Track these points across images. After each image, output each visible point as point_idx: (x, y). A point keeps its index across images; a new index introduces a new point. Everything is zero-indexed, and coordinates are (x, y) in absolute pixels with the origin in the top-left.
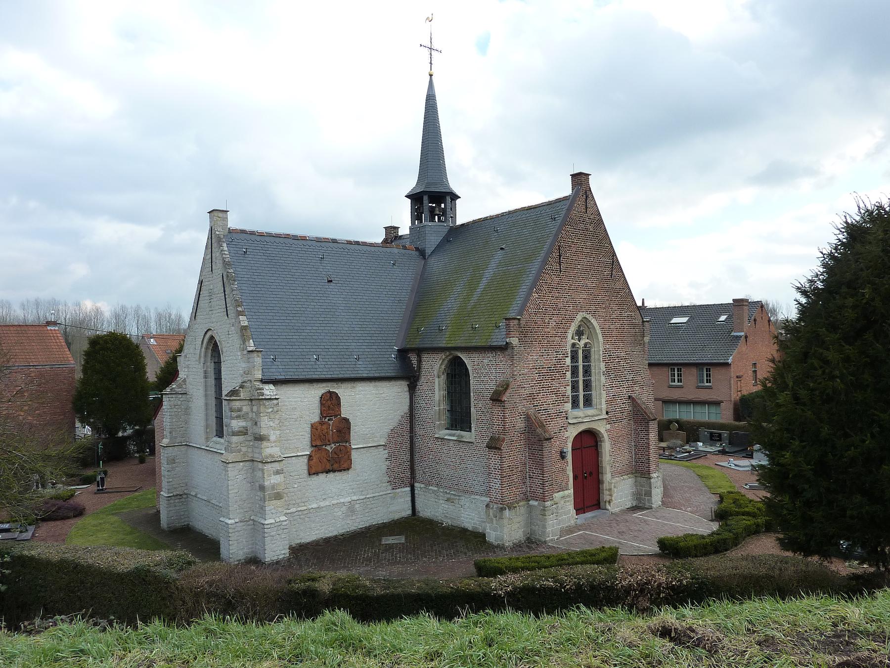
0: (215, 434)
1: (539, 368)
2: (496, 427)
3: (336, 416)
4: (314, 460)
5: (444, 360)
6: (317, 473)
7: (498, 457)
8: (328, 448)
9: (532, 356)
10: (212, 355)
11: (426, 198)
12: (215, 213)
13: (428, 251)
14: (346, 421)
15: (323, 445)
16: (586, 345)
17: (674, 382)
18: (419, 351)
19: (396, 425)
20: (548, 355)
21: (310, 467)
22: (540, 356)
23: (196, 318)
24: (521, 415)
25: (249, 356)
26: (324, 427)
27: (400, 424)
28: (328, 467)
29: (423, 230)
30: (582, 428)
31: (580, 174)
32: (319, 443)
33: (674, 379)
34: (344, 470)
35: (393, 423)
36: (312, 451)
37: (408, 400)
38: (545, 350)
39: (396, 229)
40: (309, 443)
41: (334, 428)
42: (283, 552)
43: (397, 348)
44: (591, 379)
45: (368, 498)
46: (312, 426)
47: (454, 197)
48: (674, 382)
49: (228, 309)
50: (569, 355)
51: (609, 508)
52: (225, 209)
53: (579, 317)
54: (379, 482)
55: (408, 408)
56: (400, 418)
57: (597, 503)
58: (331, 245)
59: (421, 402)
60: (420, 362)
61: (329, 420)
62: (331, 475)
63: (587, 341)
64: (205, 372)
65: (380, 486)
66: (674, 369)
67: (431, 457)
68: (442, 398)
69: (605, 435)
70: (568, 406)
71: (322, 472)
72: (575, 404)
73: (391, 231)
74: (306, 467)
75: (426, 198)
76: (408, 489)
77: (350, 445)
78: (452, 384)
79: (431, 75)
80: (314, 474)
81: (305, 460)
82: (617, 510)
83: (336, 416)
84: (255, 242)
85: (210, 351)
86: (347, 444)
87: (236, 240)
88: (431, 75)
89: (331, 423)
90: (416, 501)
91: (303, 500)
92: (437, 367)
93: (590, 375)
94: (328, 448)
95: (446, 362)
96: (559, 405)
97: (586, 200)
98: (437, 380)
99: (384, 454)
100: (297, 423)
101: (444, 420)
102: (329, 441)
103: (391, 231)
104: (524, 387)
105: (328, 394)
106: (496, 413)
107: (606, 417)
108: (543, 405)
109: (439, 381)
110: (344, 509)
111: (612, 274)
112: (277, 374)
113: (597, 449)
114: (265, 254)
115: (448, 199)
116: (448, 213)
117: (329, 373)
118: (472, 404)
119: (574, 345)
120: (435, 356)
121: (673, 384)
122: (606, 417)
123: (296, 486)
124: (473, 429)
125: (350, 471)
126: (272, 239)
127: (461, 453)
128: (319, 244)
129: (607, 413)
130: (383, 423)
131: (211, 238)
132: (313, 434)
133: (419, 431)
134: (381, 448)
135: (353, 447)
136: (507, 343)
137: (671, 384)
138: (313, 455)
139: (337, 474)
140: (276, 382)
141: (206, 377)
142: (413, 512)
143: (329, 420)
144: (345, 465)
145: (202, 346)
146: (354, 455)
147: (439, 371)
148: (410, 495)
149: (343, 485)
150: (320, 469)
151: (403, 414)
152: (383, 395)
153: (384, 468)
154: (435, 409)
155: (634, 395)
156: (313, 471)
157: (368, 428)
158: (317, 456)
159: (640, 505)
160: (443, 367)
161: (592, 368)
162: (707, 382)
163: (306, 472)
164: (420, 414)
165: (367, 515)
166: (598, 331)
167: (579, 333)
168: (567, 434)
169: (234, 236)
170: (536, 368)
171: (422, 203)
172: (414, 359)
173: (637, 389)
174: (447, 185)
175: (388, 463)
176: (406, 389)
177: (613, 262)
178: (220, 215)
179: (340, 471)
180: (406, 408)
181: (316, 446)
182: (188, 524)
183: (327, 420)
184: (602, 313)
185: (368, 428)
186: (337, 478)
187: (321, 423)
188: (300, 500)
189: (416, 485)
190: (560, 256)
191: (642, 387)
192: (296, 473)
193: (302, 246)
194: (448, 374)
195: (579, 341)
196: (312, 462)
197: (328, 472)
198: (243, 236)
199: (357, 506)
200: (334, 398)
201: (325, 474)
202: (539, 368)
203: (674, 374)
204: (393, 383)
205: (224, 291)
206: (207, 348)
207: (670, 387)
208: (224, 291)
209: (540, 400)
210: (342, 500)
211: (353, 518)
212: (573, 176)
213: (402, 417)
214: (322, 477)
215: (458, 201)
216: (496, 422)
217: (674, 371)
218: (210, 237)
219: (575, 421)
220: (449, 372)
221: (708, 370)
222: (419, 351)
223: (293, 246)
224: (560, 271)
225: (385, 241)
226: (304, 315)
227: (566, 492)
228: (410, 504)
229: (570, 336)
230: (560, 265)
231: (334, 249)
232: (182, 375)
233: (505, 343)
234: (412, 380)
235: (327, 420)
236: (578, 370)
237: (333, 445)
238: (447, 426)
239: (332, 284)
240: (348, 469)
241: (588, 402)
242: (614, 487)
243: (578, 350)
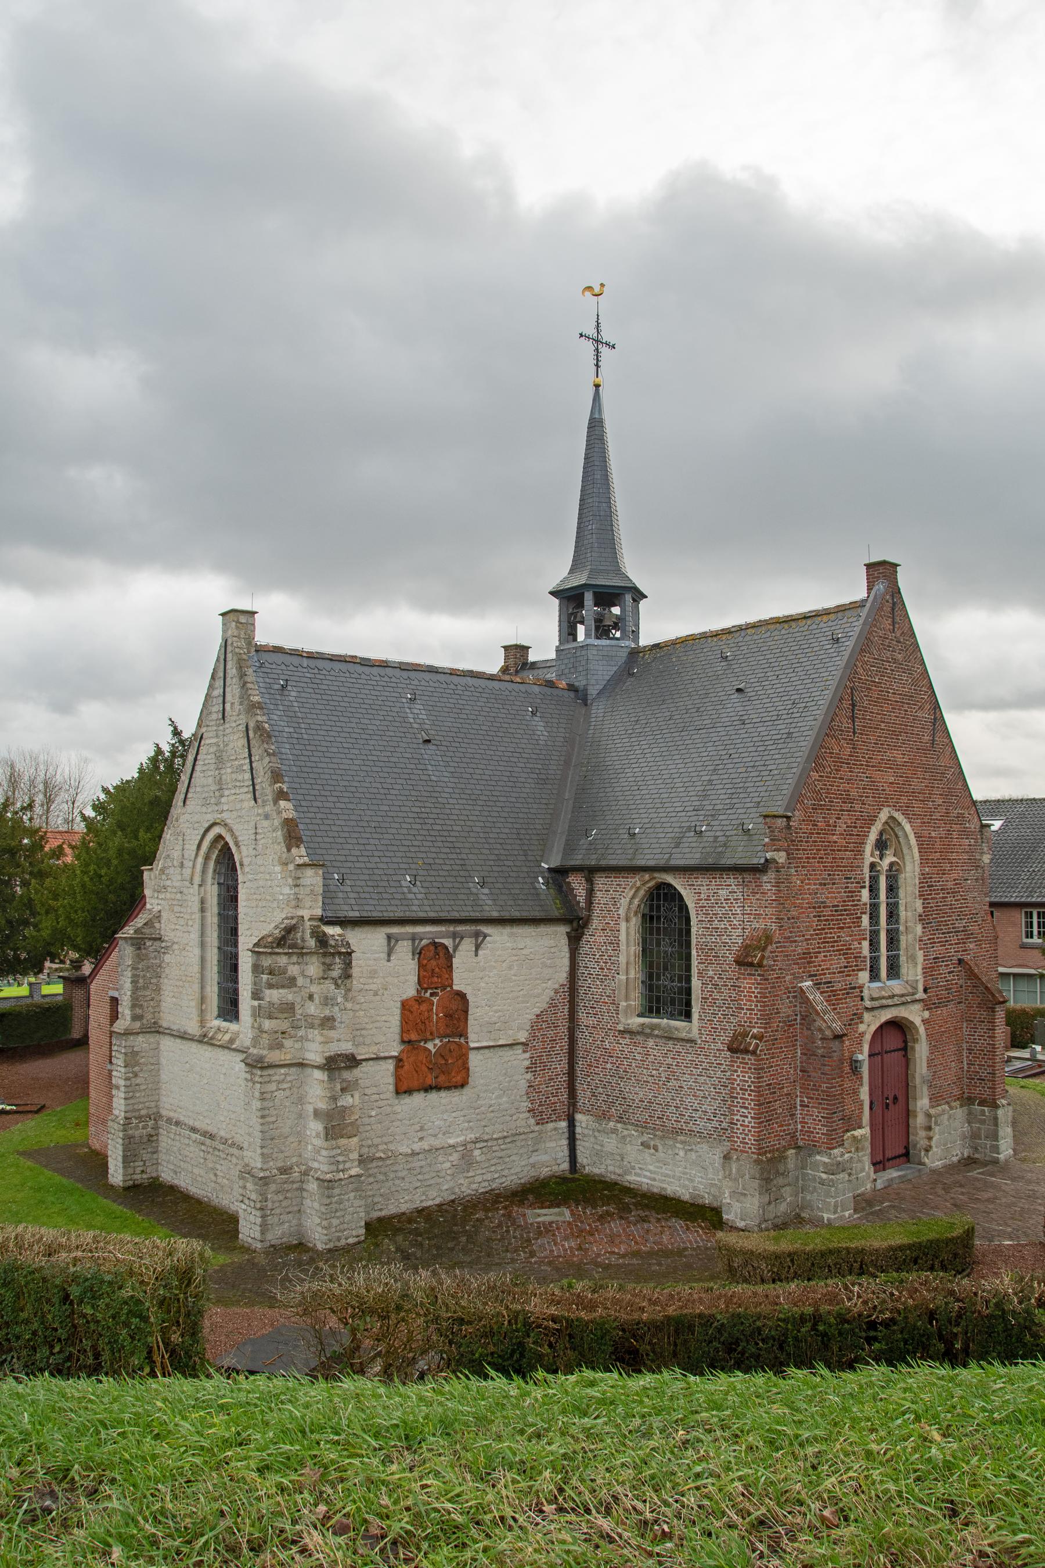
0: (216, 1013)
1: (819, 907)
2: (745, 1014)
3: (444, 988)
4: (405, 1068)
5: (638, 889)
6: (409, 1092)
7: (750, 1068)
8: (430, 1046)
9: (809, 884)
10: (215, 871)
11: (589, 598)
12: (231, 616)
13: (593, 691)
14: (462, 996)
15: (420, 1041)
16: (892, 864)
17: (1032, 937)
18: (590, 872)
19: (545, 1006)
20: (834, 884)
21: (398, 1079)
22: (821, 884)
23: (188, 802)
24: (790, 992)
25: (299, 874)
26: (424, 1007)
27: (552, 1005)
28: (430, 1080)
29: (583, 653)
30: (886, 1016)
31: (883, 563)
32: (414, 1036)
33: (1032, 932)
34: (456, 1087)
35: (541, 1004)
36: (402, 1051)
37: (566, 962)
38: (829, 875)
39: (524, 649)
40: (397, 1037)
41: (440, 1009)
42: (354, 1233)
43: (546, 866)
44: (898, 929)
45: (496, 1139)
46: (405, 1005)
47: (639, 595)
48: (1032, 937)
49: (257, 787)
50: (867, 884)
51: (926, 1160)
52: (249, 609)
53: (884, 815)
54: (514, 1111)
55: (565, 975)
56: (552, 993)
57: (904, 1151)
58: (427, 676)
59: (589, 965)
60: (590, 893)
61: (432, 995)
62: (433, 1096)
63: (894, 859)
64: (203, 902)
65: (514, 1117)
66: (1031, 913)
67: (609, 1066)
68: (632, 958)
69: (922, 1030)
70: (864, 976)
71: (419, 1090)
72: (874, 976)
73: (517, 653)
74: (391, 1080)
75: (589, 598)
76: (564, 1124)
77: (467, 1043)
78: (651, 934)
79: (597, 386)
80: (405, 1092)
81: (390, 1066)
82: (938, 1164)
83: (444, 988)
84: (300, 669)
85: (211, 864)
86: (462, 1040)
87: (267, 664)
88: (597, 386)
89: (435, 1000)
90: (578, 1147)
91: (385, 1139)
92: (624, 902)
93: (897, 922)
94: (430, 1046)
95: (642, 893)
96: (849, 976)
97: (893, 609)
98: (623, 926)
99: (520, 1059)
100: (378, 998)
101: (636, 1000)
102: (431, 1034)
103: (517, 653)
104: (795, 941)
105: (432, 948)
106: (745, 988)
107: (925, 996)
108: (825, 974)
109: (628, 928)
110: (455, 1157)
111: (933, 740)
112: (346, 908)
113: (905, 1056)
114: (317, 691)
115: (628, 598)
116: (629, 626)
117: (378, 908)
118: (694, 971)
119: (873, 866)
120: (622, 881)
121: (1029, 940)
122: (925, 996)
123: (373, 1113)
124: (695, 1016)
125: (466, 1090)
126: (327, 665)
127: (669, 1061)
128: (405, 674)
129: (925, 991)
130: (523, 1002)
131: (225, 660)
132: (405, 1021)
133: (584, 1018)
134: (519, 1050)
135: (472, 1045)
136: (767, 860)
137: (1025, 940)
138: (405, 1059)
139: (443, 1094)
140: (344, 923)
141: (203, 910)
142: (571, 1166)
143: (432, 995)
144: (458, 1079)
145: (197, 855)
146: (475, 1060)
147: (629, 908)
148: (567, 1135)
149: (454, 1115)
150: (415, 1084)
151: (557, 986)
152: (524, 952)
153: (523, 1085)
154: (619, 980)
155: (967, 958)
156: (404, 1088)
157: (496, 1012)
158: (412, 1059)
159: (976, 1156)
160: (636, 902)
161: (902, 908)
162: (1027, 937)
163: (392, 1088)
164: (590, 987)
165: (493, 1169)
166: (913, 841)
167: (881, 845)
168: (862, 1028)
169: (265, 657)
170: (814, 908)
171: (581, 605)
172: (578, 885)
173: (972, 946)
174: (618, 571)
175: (529, 1076)
176: (564, 941)
177: (935, 719)
178: (243, 619)
179: (448, 1088)
180: (562, 975)
181: (409, 1042)
182: (157, 1178)
183: (428, 995)
184: (917, 807)
185: (496, 1012)
186: (443, 1101)
187: (419, 1000)
188: (379, 1140)
189: (579, 1117)
190: (853, 705)
191: (978, 943)
192: (374, 1090)
193: (378, 678)
194: (644, 916)
195: (881, 859)
196: (402, 1072)
197: (428, 1089)
198: (279, 658)
199: (477, 1153)
200: (441, 955)
201: (422, 1094)
202: (819, 907)
203: (1031, 923)
204: (543, 929)
205: (250, 755)
206: (207, 858)
207: (1024, 946)
208: (250, 755)
209: (820, 966)
210: (451, 1141)
211: (470, 1174)
212: (869, 566)
213: (556, 992)
214: (418, 1099)
215: (643, 604)
216: (745, 1005)
217: (1031, 917)
218: (222, 657)
219: (876, 1004)
220: (647, 911)
221: (590, 881)
222: (590, 872)
223: (332, 673)
224: (854, 733)
225: (505, 670)
226: (385, 802)
227: (858, 1133)
228: (566, 1152)
229: (868, 848)
230: (853, 721)
231: (431, 683)
232: (153, 902)
233: (762, 861)
234: (575, 924)
235: (428, 995)
236: (879, 912)
237: (437, 1041)
238: (639, 1010)
239: (430, 746)
240: (462, 1086)
241: (894, 970)
242: (936, 1123)
243: (878, 876)
